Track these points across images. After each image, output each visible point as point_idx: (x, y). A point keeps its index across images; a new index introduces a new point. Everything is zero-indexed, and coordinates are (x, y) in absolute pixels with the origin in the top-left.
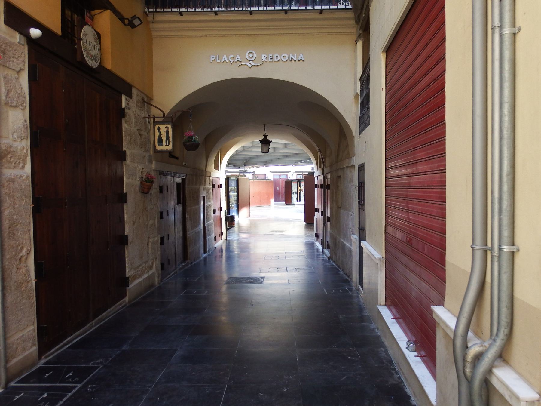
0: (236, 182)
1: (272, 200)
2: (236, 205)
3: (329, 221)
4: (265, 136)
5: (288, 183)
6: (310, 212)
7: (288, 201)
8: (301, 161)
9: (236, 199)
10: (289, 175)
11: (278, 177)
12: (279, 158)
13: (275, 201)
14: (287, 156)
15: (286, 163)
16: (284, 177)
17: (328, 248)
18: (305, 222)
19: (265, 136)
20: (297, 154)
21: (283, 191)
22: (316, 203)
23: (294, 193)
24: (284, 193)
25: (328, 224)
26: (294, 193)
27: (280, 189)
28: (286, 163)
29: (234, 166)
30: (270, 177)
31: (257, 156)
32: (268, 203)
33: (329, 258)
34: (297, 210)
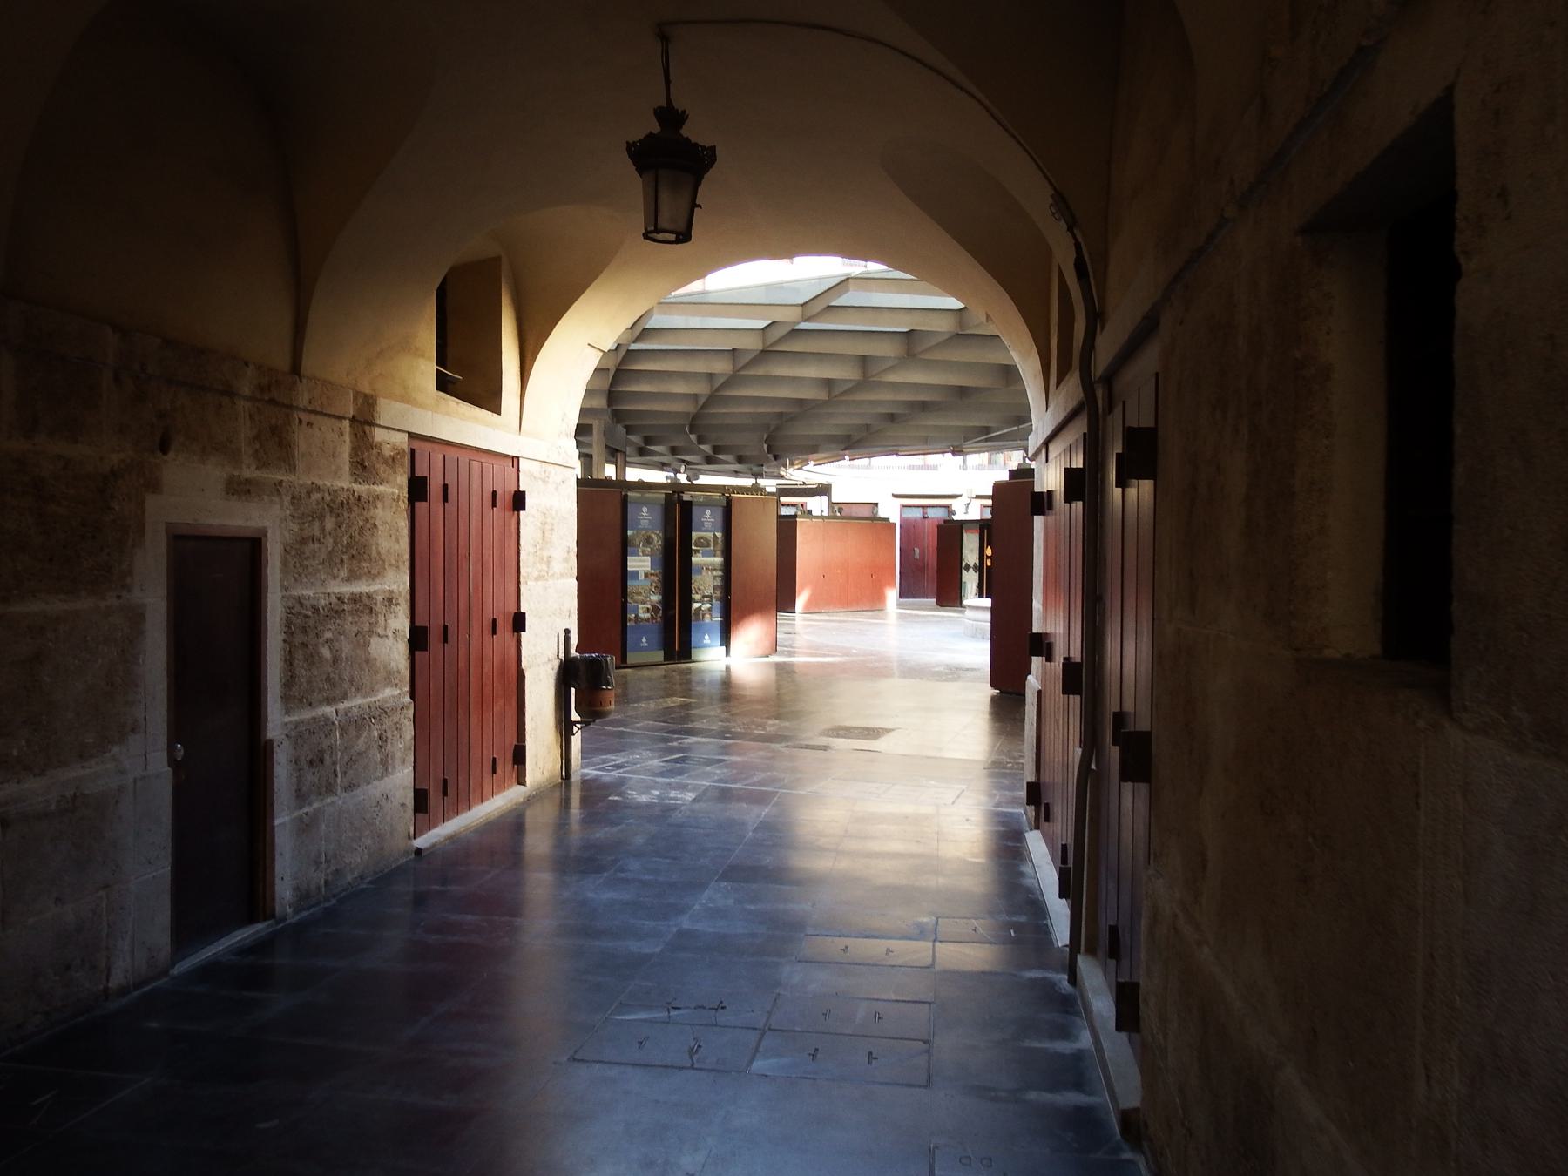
0: (719, 513)
1: (892, 594)
2: (717, 604)
3: (1138, 764)
4: (671, 117)
5: (951, 532)
6: (1013, 648)
7: (949, 595)
8: (987, 430)
9: (718, 582)
10: (957, 505)
11: (918, 514)
12: (892, 418)
13: (903, 594)
14: (924, 406)
15: (925, 440)
16: (937, 515)
17: (1114, 951)
18: (993, 684)
19: (671, 117)
20: (962, 391)
21: (932, 560)
22: (1037, 605)
23: (967, 568)
24: (931, 562)
25: (1130, 802)
26: (967, 568)
27: (922, 553)
28: (927, 443)
29: (740, 460)
30: (891, 511)
31: (801, 402)
32: (874, 601)
33: (1129, 1121)
34: (962, 637)
